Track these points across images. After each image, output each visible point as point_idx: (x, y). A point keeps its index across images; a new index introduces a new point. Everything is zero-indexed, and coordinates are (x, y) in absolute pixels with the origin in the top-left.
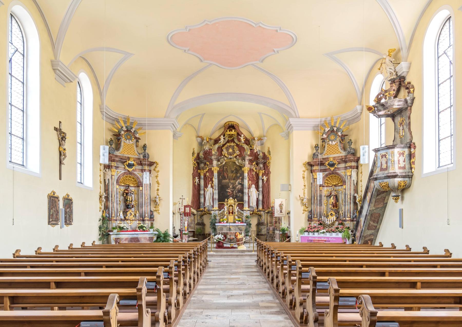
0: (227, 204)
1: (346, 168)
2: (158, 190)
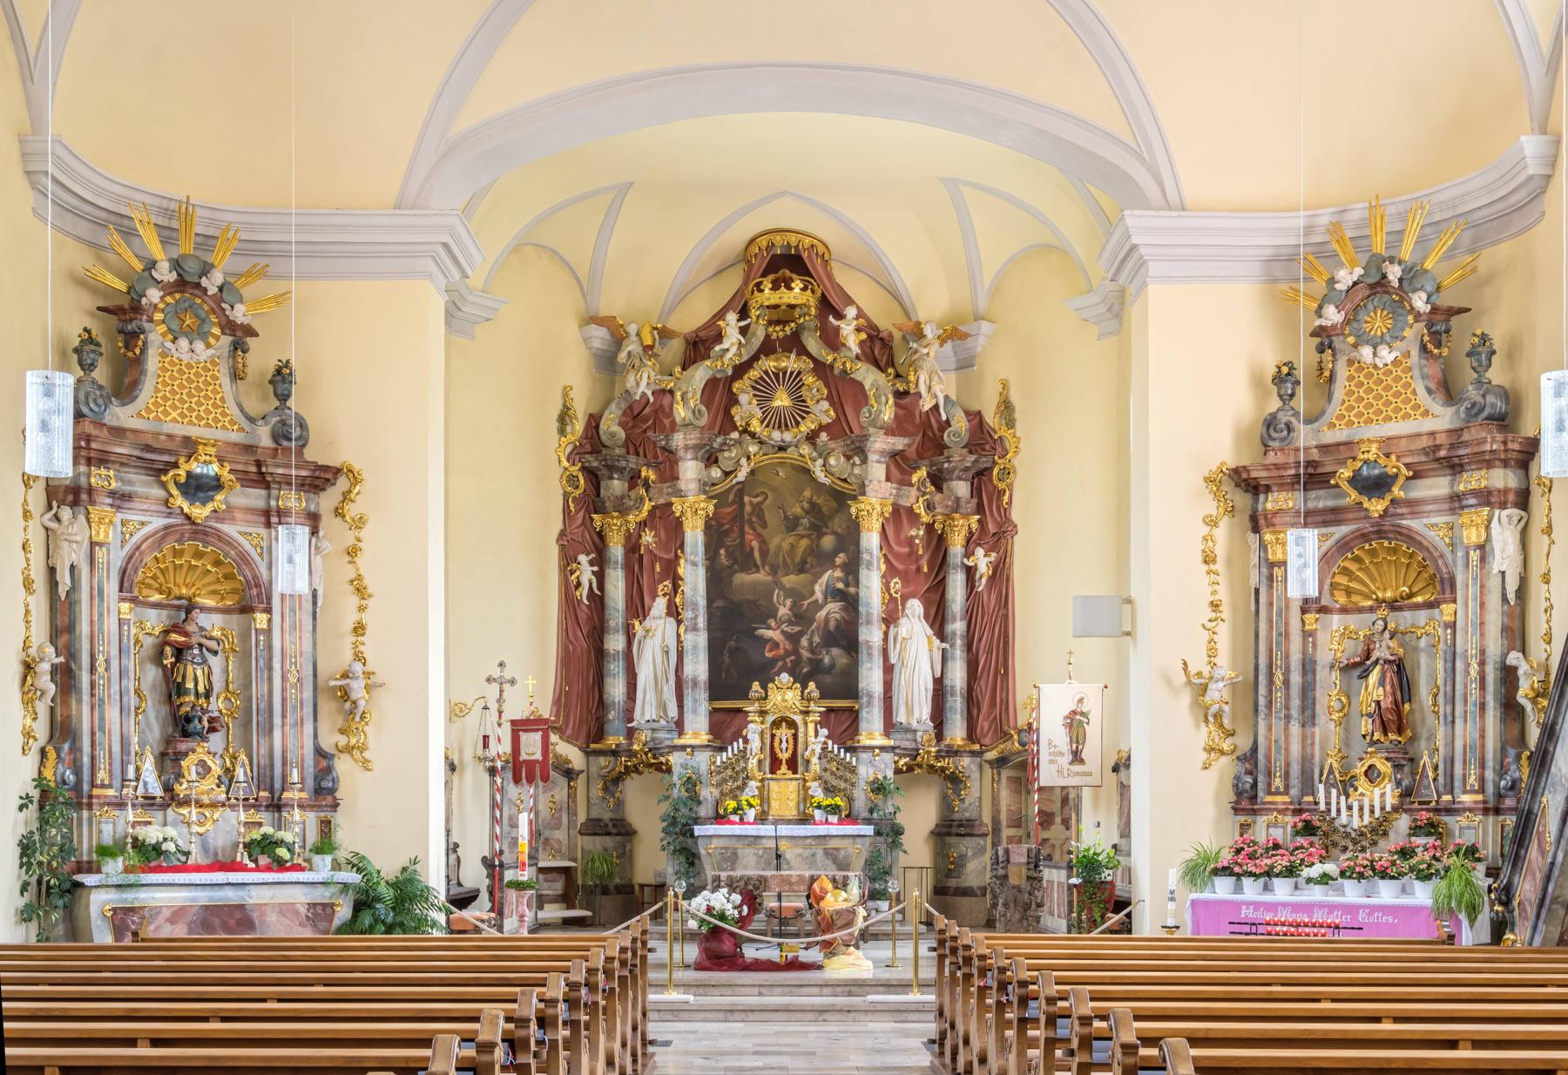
0: (763, 713)
1: (1456, 502)
2: (359, 629)
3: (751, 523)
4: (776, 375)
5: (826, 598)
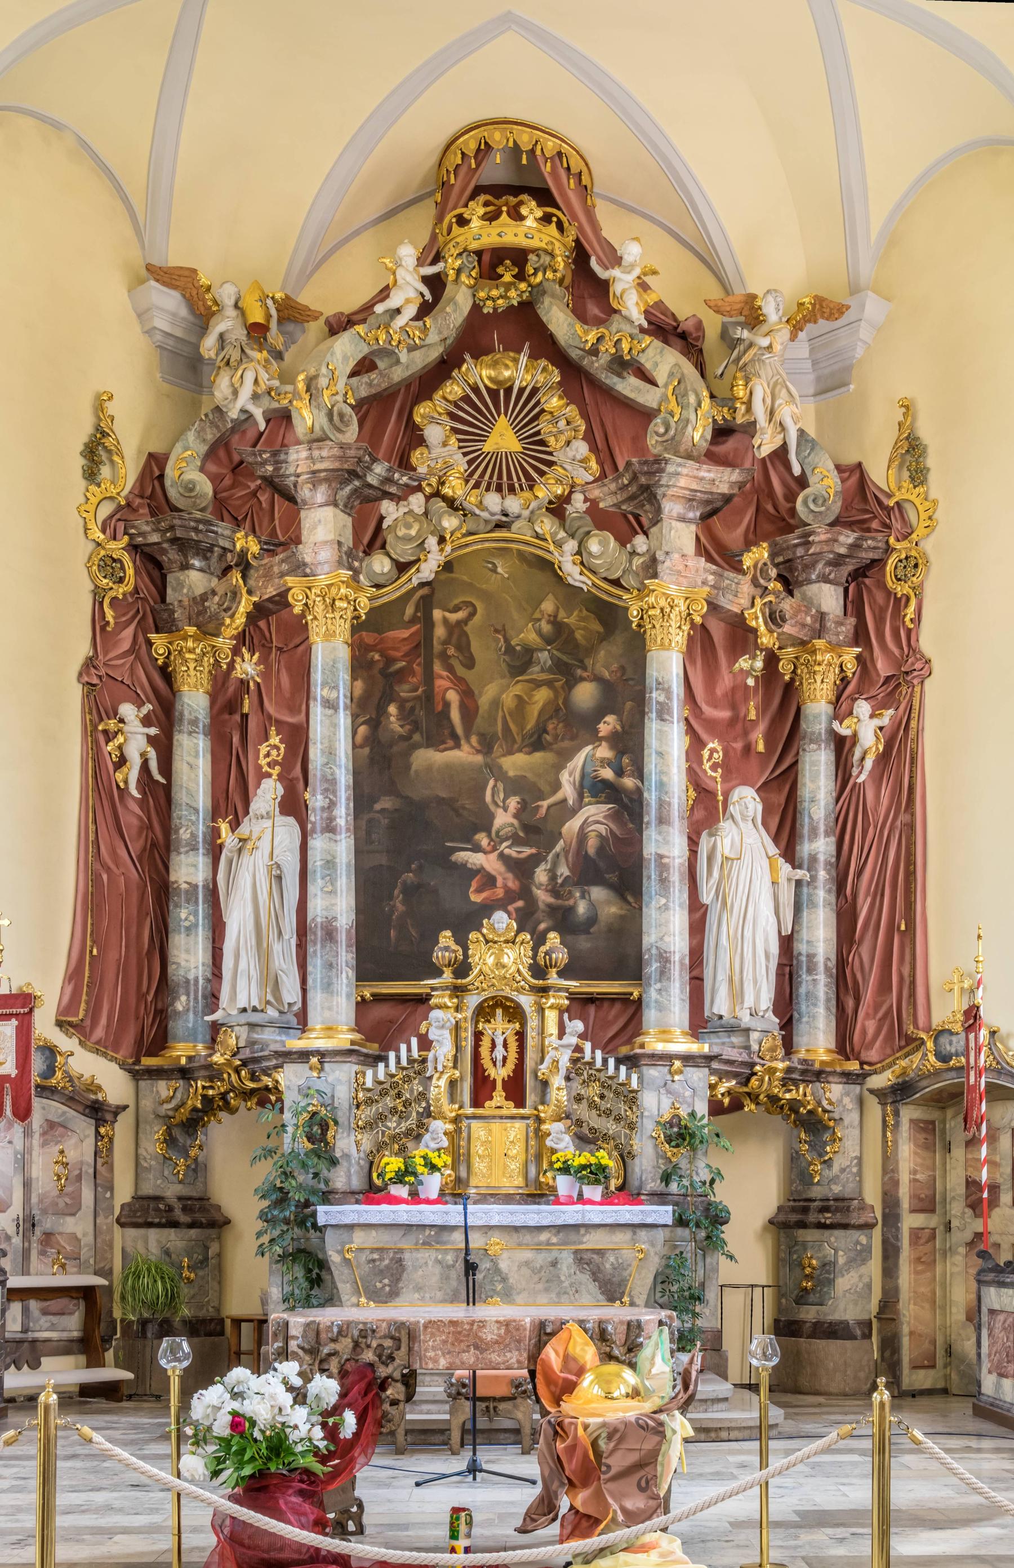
0: (458, 991)
3: (444, 657)
4: (494, 394)
5: (581, 796)
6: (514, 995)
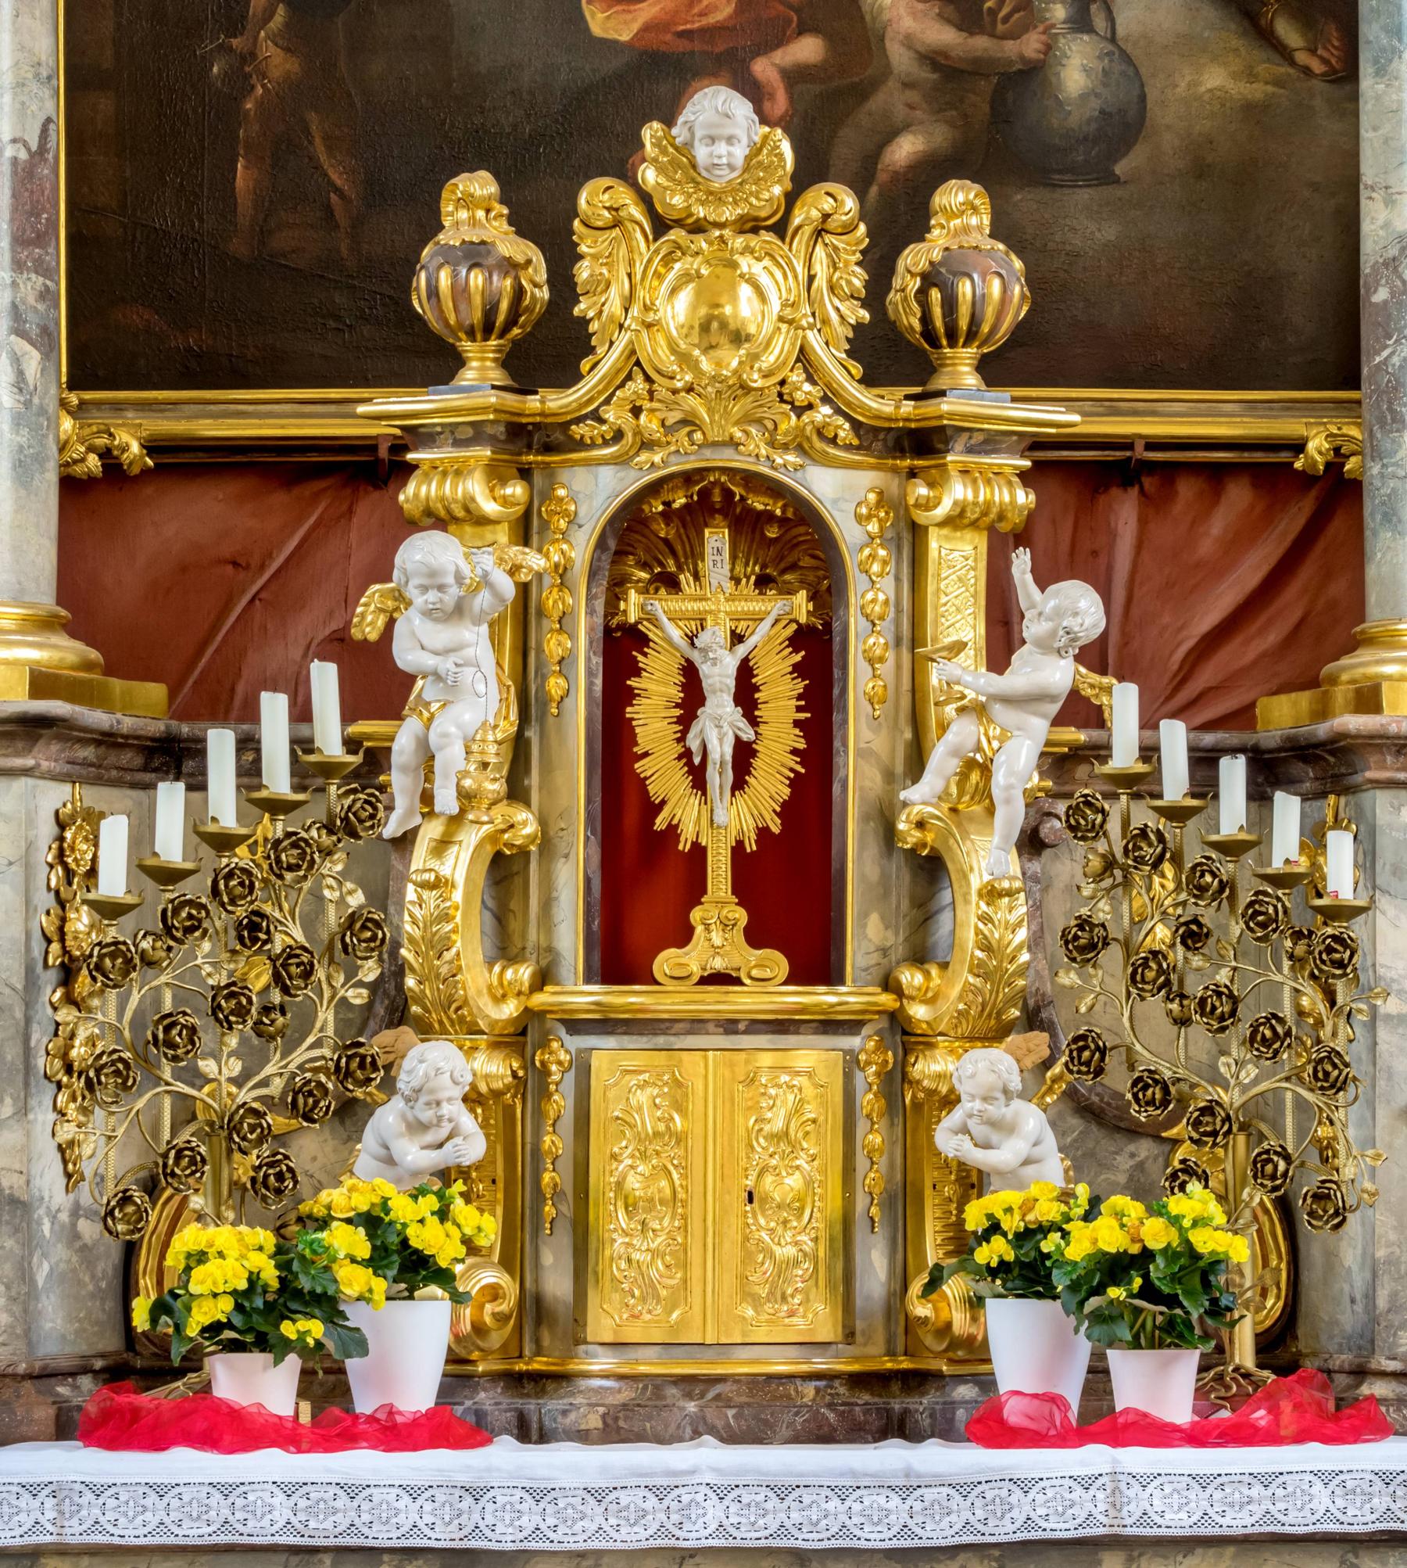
0: (529, 447)
6: (785, 467)
